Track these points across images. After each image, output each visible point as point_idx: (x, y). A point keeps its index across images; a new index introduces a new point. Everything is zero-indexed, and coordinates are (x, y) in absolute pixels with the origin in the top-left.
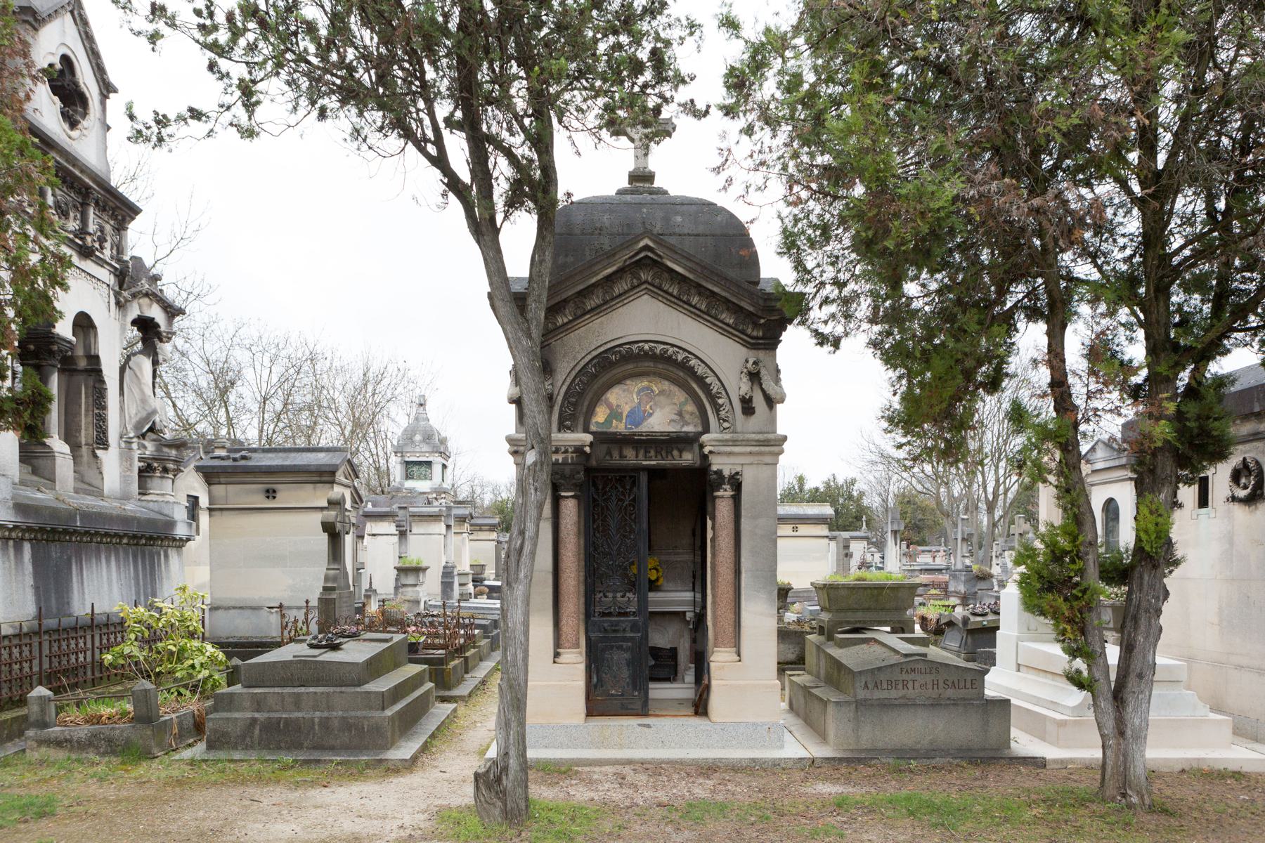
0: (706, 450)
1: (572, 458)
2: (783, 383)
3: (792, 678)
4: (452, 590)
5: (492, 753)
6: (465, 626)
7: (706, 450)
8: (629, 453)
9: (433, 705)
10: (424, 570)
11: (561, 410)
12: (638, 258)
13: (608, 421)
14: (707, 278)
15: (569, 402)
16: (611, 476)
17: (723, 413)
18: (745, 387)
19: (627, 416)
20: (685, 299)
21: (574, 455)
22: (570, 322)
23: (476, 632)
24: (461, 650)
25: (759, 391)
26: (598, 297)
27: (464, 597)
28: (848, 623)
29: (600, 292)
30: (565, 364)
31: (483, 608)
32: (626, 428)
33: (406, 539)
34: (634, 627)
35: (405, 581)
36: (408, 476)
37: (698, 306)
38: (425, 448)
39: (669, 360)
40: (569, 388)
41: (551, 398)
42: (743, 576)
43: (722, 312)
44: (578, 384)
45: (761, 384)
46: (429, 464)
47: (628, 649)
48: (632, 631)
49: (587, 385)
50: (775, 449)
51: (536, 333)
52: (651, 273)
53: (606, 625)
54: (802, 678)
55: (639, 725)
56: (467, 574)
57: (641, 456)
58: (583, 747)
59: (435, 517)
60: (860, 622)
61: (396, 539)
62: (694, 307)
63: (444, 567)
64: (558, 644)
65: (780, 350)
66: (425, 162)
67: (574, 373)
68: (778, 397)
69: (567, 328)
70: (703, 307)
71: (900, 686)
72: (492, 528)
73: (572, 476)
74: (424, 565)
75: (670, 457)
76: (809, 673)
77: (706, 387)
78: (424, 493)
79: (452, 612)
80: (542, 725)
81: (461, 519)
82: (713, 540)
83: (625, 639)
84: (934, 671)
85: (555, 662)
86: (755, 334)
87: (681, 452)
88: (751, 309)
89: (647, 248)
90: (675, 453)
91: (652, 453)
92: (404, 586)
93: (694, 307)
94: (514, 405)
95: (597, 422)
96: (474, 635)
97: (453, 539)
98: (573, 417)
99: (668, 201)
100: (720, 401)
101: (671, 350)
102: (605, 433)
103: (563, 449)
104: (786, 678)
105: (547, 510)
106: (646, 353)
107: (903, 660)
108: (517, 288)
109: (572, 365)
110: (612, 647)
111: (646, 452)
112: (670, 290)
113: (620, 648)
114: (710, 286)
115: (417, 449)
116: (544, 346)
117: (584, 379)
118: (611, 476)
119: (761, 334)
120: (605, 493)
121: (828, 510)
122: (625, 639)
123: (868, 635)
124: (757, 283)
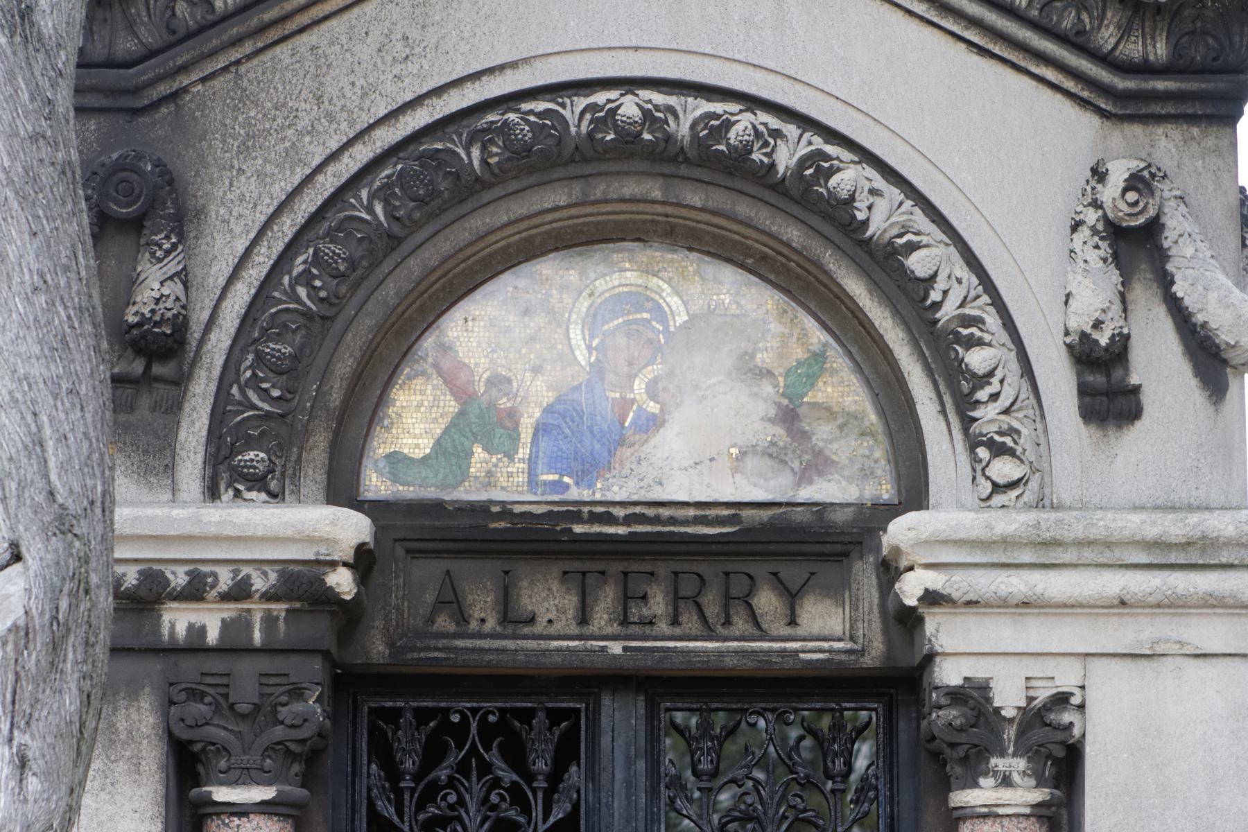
0: (911, 588)
1: (269, 621)
7: (911, 588)
16: (458, 707)
17: (988, 416)
19: (541, 430)
21: (280, 608)
25: (1161, 312)
32: (532, 482)
44: (306, 278)
45: (1165, 281)
57: (601, 618)
67: (287, 227)
73: (263, 712)
75: (741, 624)
86: (1133, 50)
87: (792, 597)
90: (767, 601)
95: (395, 459)
100: (977, 359)
101: (744, 124)
102: (436, 508)
103: (225, 579)
106: (628, 141)
109: (279, 191)
111: (629, 597)
118: (458, 707)
120: (430, 794)
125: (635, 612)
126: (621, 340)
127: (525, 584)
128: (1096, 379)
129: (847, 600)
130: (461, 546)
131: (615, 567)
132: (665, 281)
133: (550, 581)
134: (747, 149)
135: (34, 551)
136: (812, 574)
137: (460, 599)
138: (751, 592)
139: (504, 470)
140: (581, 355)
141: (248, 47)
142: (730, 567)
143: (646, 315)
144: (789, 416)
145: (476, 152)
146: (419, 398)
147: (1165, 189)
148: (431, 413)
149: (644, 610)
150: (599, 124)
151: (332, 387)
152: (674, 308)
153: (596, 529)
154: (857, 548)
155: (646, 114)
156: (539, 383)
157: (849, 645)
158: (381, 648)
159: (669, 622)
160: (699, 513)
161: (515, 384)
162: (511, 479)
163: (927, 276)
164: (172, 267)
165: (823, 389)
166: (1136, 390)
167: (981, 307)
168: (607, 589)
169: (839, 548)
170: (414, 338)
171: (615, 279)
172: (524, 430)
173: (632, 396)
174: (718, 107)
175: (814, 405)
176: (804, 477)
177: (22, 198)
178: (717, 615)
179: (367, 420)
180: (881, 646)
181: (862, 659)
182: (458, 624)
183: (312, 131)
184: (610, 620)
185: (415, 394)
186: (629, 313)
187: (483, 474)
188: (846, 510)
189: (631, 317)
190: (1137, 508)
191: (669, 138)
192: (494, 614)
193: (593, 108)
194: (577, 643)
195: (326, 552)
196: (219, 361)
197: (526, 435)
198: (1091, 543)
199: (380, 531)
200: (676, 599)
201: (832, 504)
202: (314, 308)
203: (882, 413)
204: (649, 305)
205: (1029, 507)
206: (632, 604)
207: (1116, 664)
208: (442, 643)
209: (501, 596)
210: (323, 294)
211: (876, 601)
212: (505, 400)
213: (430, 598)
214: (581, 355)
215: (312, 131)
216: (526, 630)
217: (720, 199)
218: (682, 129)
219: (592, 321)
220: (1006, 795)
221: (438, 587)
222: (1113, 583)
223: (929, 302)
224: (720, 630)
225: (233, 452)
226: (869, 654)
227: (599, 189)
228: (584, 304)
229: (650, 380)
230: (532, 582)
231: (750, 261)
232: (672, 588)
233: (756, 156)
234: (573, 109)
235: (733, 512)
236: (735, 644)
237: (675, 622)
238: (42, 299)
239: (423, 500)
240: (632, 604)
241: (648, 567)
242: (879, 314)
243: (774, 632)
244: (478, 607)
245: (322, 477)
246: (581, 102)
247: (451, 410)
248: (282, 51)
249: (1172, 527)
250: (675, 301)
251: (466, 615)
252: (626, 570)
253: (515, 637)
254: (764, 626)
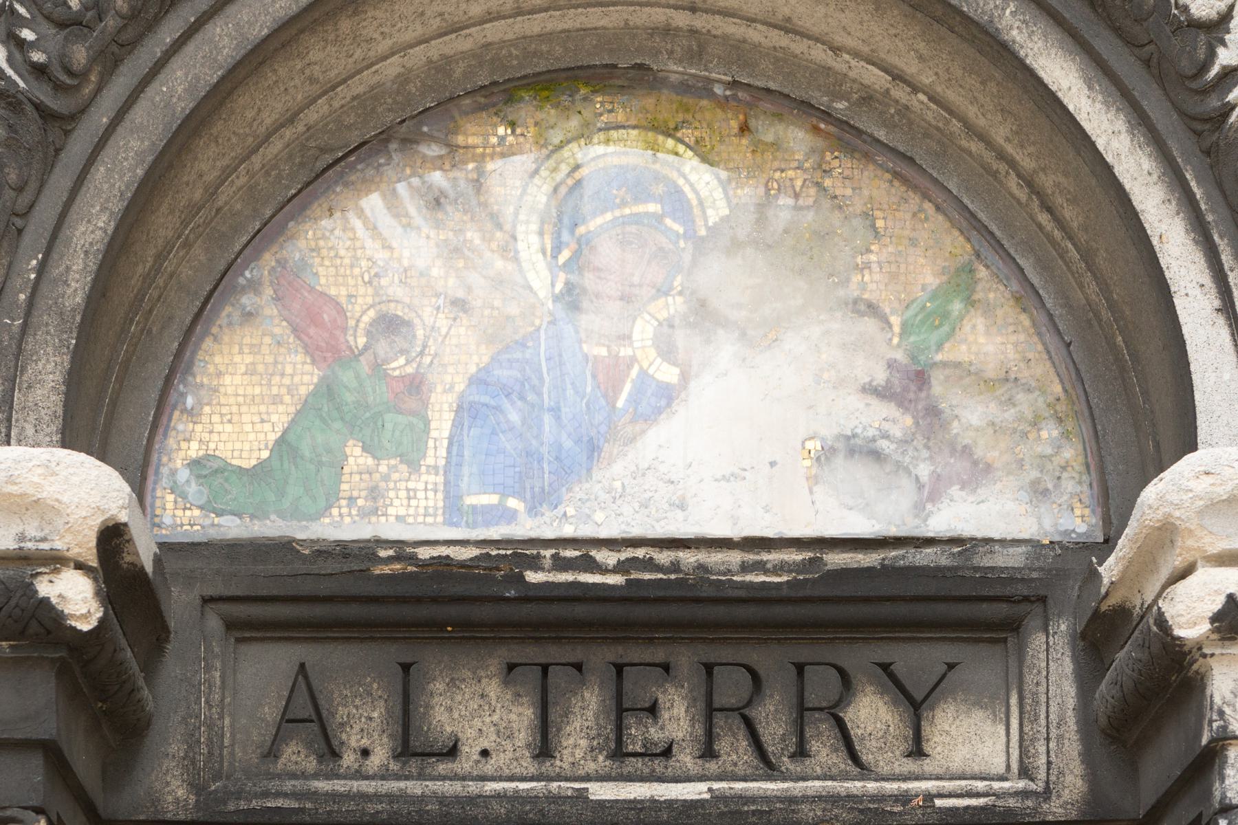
19: (466, 412)
32: (453, 508)
75: (824, 752)
102: (284, 548)
125: (638, 734)
127: (439, 686)
129: (1014, 700)
130: (320, 611)
131: (601, 656)
132: (688, 146)
133: (484, 681)
136: (951, 666)
137: (325, 713)
139: (403, 485)
142: (804, 653)
143: (653, 207)
146: (249, 359)
148: (269, 385)
149: (652, 730)
151: (68, 269)
152: (704, 193)
154: (1037, 609)
156: (462, 330)
157: (1021, 784)
158: (180, 793)
159: (697, 753)
160: (751, 557)
161: (420, 333)
162: (414, 503)
163: (1213, 15)
165: (971, 338)
168: (587, 695)
169: (1003, 609)
170: (238, 247)
172: (437, 415)
173: (629, 352)
178: (783, 739)
179: (154, 395)
180: (1079, 783)
181: (1045, 806)
182: (321, 758)
184: (592, 750)
185: (241, 352)
186: (624, 204)
187: (363, 494)
188: (1011, 550)
189: (627, 211)
192: (385, 740)
194: (533, 784)
195: (39, 535)
197: (441, 425)
200: (710, 712)
201: (988, 541)
202: (22, 84)
204: (660, 189)
206: (630, 720)
208: (289, 785)
209: (398, 710)
210: (37, 57)
211: (1071, 702)
212: (402, 361)
216: (443, 767)
221: (286, 693)
223: (1215, 70)
224: (787, 764)
226: (1059, 796)
229: (659, 355)
230: (453, 683)
231: (841, 105)
232: (703, 690)
235: (808, 555)
236: (817, 783)
237: (708, 752)
239: (255, 539)
240: (630, 720)
241: (659, 655)
242: (1106, 125)
243: (885, 769)
244: (357, 728)
247: (306, 378)
251: (335, 743)
252: (619, 661)
253: (421, 777)
254: (866, 758)
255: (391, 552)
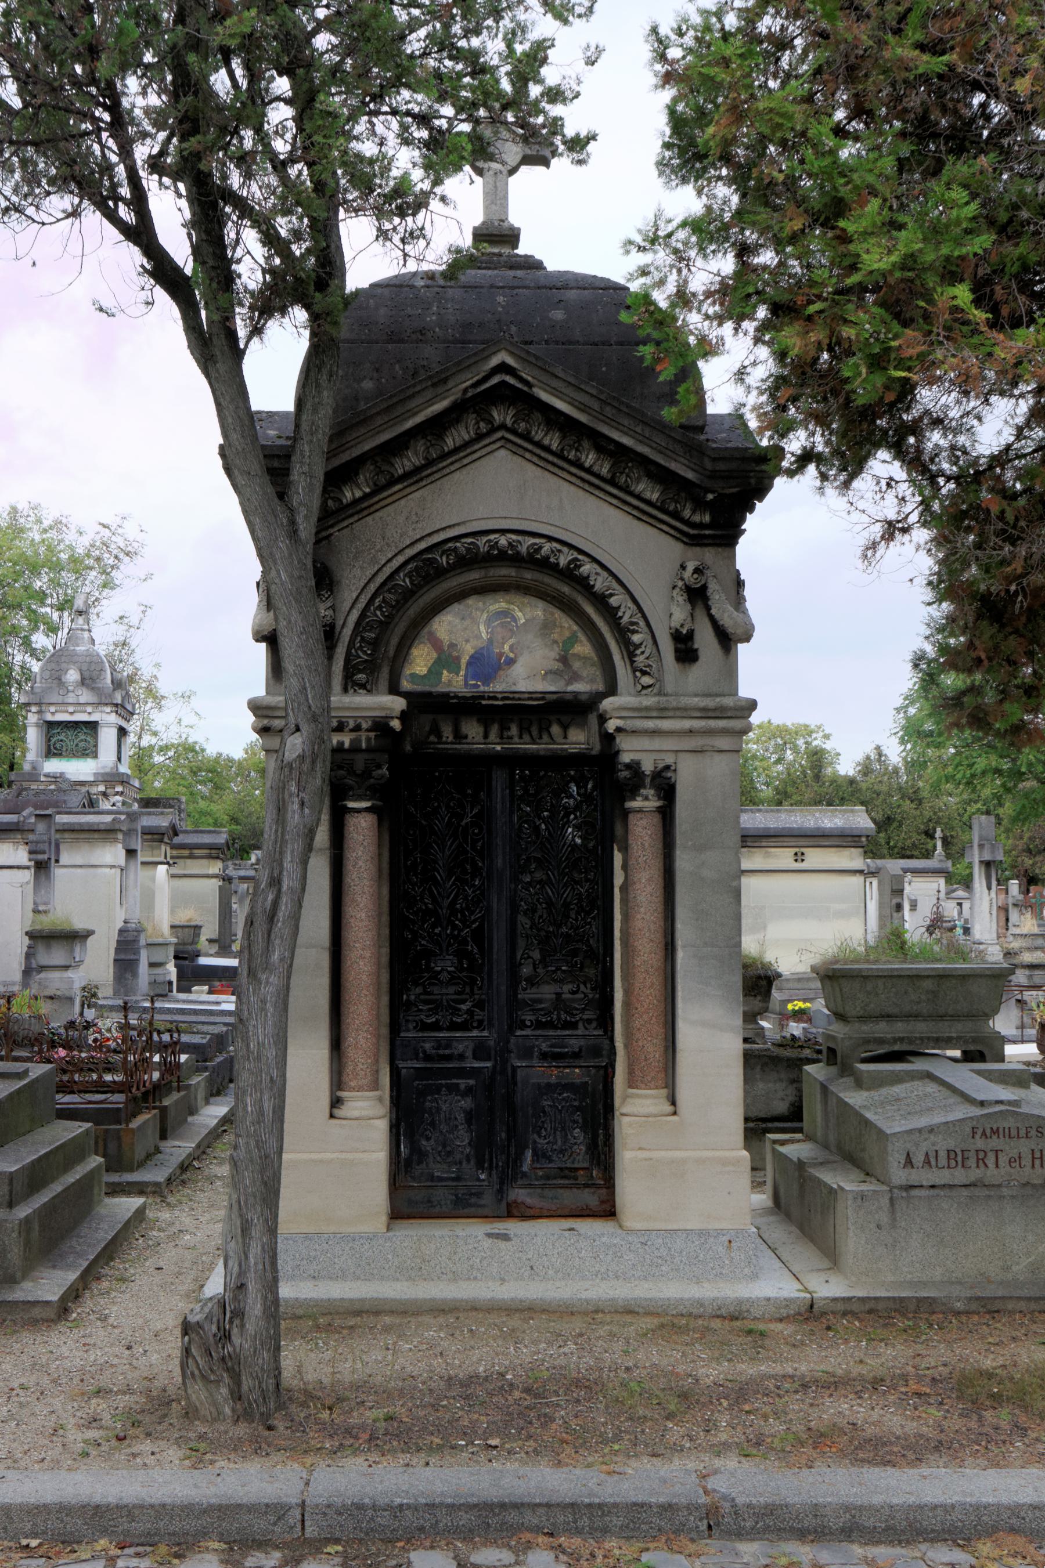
0: (611, 725)
1: (368, 739)
2: (749, 605)
3: (782, 1149)
4: (135, 974)
5: (215, 1285)
6: (163, 1048)
7: (611, 725)
8: (473, 730)
9: (100, 1201)
10: (89, 933)
11: (348, 654)
12: (487, 385)
13: (434, 672)
14: (611, 422)
15: (363, 638)
17: (640, 660)
18: (679, 614)
19: (469, 664)
20: (572, 456)
21: (372, 734)
22: (366, 497)
23: (183, 1058)
24: (157, 1090)
26: (416, 454)
27: (161, 991)
28: (881, 1041)
29: (420, 446)
30: (358, 572)
31: (195, 1012)
32: (466, 684)
33: (48, 876)
34: (480, 1051)
35: (43, 958)
36: (51, 751)
37: (596, 469)
38: (85, 696)
39: (545, 565)
40: (363, 615)
41: (330, 634)
42: (680, 955)
43: (638, 480)
44: (380, 608)
45: (708, 609)
46: (92, 727)
47: (469, 1090)
48: (476, 1057)
49: (399, 606)
50: (736, 724)
51: (306, 529)
52: (511, 412)
53: (427, 1046)
54: (796, 1149)
55: (489, 1235)
56: (166, 944)
57: (493, 736)
58: (382, 1278)
59: (105, 833)
60: (901, 1040)
61: (28, 876)
62: (589, 471)
63: (121, 931)
64: (338, 1081)
65: (744, 548)
66: (112, 233)
67: (372, 588)
68: (739, 631)
69: (360, 508)
70: (605, 471)
71: (972, 1162)
72: (215, 852)
73: (367, 774)
74: (79, 924)
75: (545, 738)
76: (809, 1138)
77: (611, 614)
78: (82, 783)
79: (140, 1019)
80: (307, 1236)
81: (155, 836)
82: (624, 888)
83: (463, 1073)
84: (1033, 1133)
85: (332, 1116)
86: (697, 518)
87: (565, 728)
88: (690, 475)
89: (503, 368)
90: (555, 729)
91: (514, 730)
92: (43, 968)
93: (589, 471)
94: (263, 646)
95: (413, 675)
96: (178, 1065)
97: (139, 874)
98: (372, 667)
99: (543, 282)
100: (636, 638)
101: (547, 547)
102: (429, 694)
103: (351, 724)
104: (768, 1145)
105: (322, 836)
107: (978, 1112)
108: (270, 434)
109: (369, 573)
110: (438, 1089)
111: (504, 728)
112: (546, 442)
113: (453, 1089)
114: (615, 435)
115: (71, 698)
116: (322, 538)
117: (391, 597)
119: (707, 518)
121: (861, 820)
122: (463, 1073)
123: (918, 1065)
124: (701, 429)
125: (505, 734)
126: (499, 629)
128: (681, 646)
134: (548, 558)
135: (305, 728)
138: (550, 726)
140: (484, 635)
141: (356, 518)
144: (564, 659)
145: (444, 558)
147: (708, 573)
150: (492, 547)
153: (491, 702)
155: (510, 544)
164: (329, 604)
166: (696, 650)
167: (638, 618)
171: (497, 606)
174: (537, 541)
175: (574, 655)
176: (569, 682)
177: (296, 600)
183: (381, 550)
190: (696, 695)
191: (518, 553)
193: (489, 541)
196: (347, 639)
197: (463, 666)
198: (678, 709)
199: (409, 704)
203: (599, 657)
205: (655, 695)
207: (688, 755)
213: (427, 729)
214: (484, 635)
215: (381, 550)
217: (538, 576)
218: (523, 549)
219: (488, 623)
220: (646, 803)
222: (687, 724)
225: (354, 675)
227: (492, 572)
228: (485, 616)
233: (552, 560)
234: (482, 542)
238: (304, 637)
245: (386, 683)
246: (485, 539)
248: (369, 519)
249: (709, 702)
250: (520, 614)
255: (119, 1078)
